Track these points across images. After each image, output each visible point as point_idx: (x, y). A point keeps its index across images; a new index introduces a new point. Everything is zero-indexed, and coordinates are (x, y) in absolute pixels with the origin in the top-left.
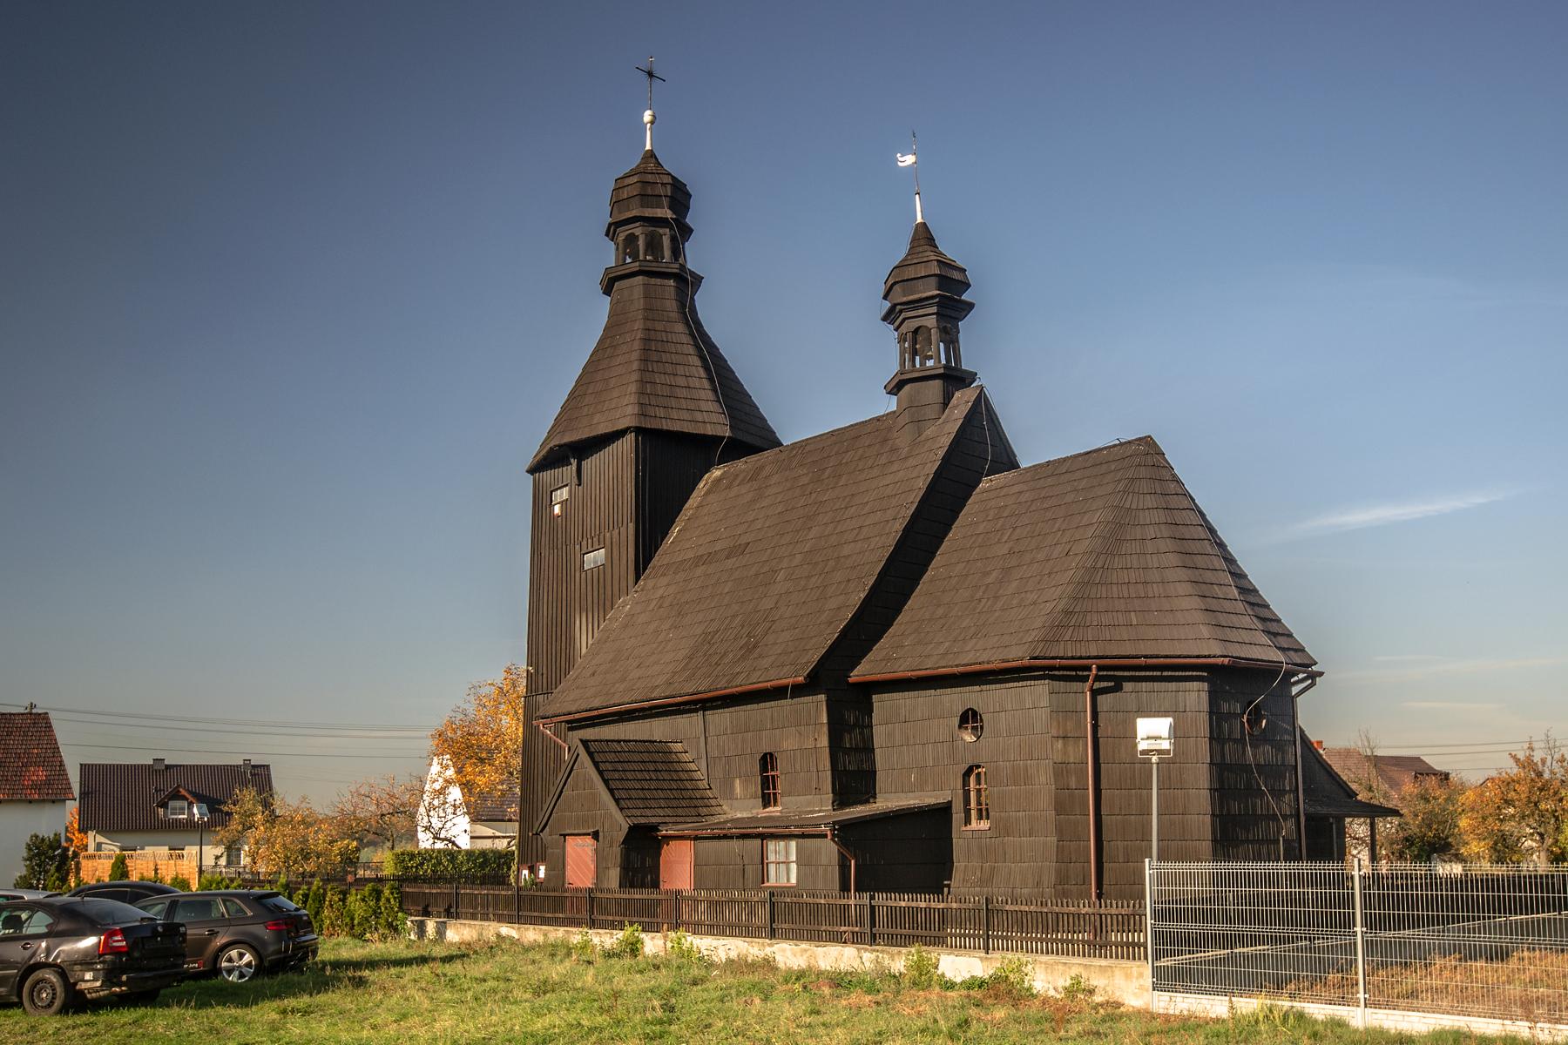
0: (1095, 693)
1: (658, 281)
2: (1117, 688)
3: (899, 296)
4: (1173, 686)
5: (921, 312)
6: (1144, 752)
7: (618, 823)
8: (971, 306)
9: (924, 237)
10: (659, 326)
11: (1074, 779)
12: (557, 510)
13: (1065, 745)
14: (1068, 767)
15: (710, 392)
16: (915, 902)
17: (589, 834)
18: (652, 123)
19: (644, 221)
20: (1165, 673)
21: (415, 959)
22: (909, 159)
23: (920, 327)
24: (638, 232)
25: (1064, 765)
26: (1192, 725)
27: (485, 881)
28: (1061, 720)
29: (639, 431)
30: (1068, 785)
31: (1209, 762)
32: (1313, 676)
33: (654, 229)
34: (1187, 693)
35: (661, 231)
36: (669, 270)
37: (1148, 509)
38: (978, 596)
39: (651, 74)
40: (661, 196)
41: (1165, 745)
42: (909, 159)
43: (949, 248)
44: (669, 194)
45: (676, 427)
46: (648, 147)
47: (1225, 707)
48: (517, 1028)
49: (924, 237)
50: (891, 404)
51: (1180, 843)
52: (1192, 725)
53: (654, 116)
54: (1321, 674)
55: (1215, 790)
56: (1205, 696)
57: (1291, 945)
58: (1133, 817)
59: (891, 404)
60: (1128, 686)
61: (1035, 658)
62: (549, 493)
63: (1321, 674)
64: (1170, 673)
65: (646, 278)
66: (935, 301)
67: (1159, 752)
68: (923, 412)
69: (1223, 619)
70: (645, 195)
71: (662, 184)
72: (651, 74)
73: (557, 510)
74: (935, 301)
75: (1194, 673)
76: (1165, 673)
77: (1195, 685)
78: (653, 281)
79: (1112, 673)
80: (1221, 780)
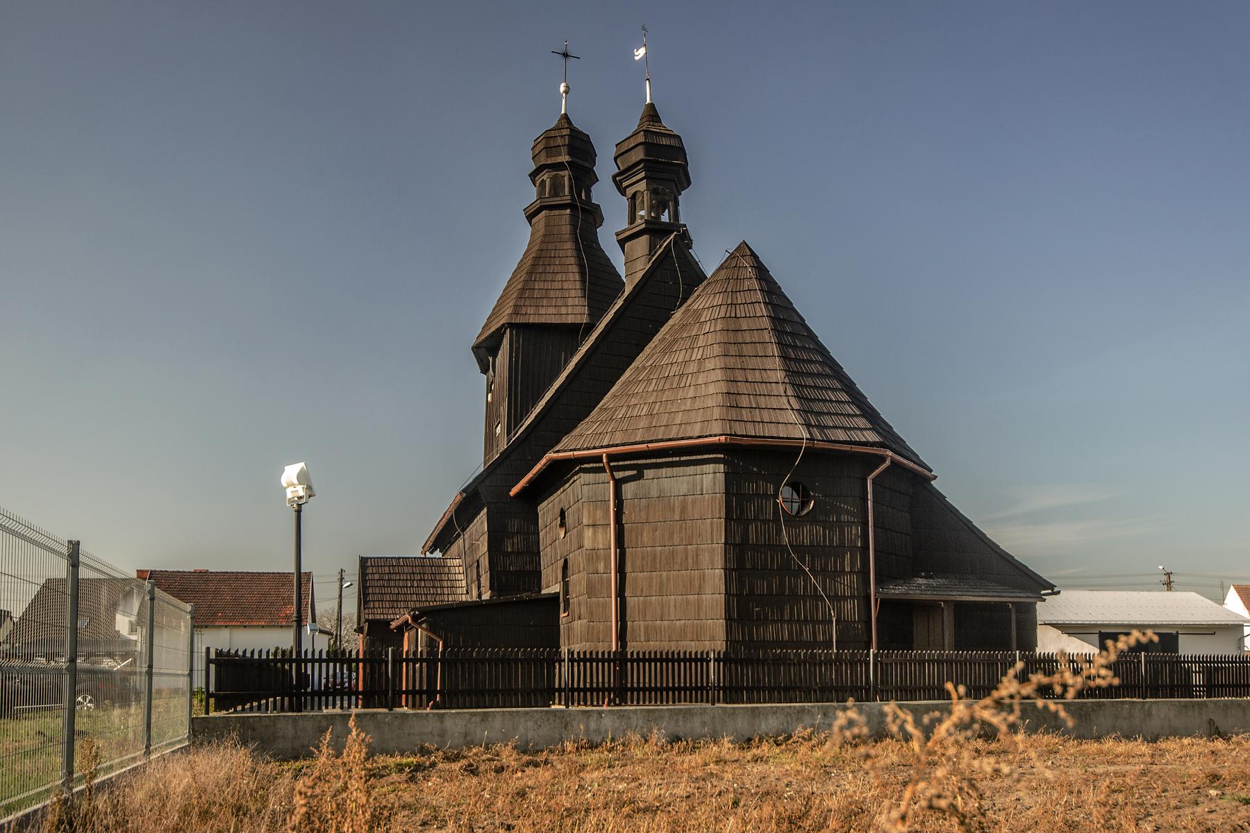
0: (618, 484)
1: (557, 212)
2: (639, 476)
3: (543, 160)
4: (690, 470)
5: (634, 179)
9: (652, 114)
10: (551, 246)
11: (602, 564)
13: (594, 533)
14: (598, 554)
15: (579, 291)
18: (566, 92)
19: (548, 168)
20: (683, 458)
22: (640, 53)
23: (636, 192)
24: (545, 177)
25: (594, 552)
26: (708, 507)
28: (591, 509)
30: (597, 570)
31: (723, 541)
33: (556, 173)
34: (704, 475)
35: (561, 173)
36: (563, 202)
39: (566, 55)
40: (560, 146)
42: (640, 53)
43: (670, 123)
44: (567, 143)
45: (543, 320)
46: (563, 112)
47: (750, 488)
48: (1228, 777)
49: (652, 114)
51: (695, 621)
52: (708, 507)
53: (567, 87)
55: (731, 570)
56: (721, 477)
57: (27, 707)
58: (653, 598)
60: (649, 473)
64: (688, 458)
65: (548, 211)
66: (640, 167)
68: (634, 266)
69: (817, 407)
70: (549, 148)
71: (562, 136)
72: (566, 55)
74: (640, 167)
75: (711, 456)
76: (683, 458)
77: (709, 468)
78: (553, 212)
79: (635, 462)
80: (740, 560)
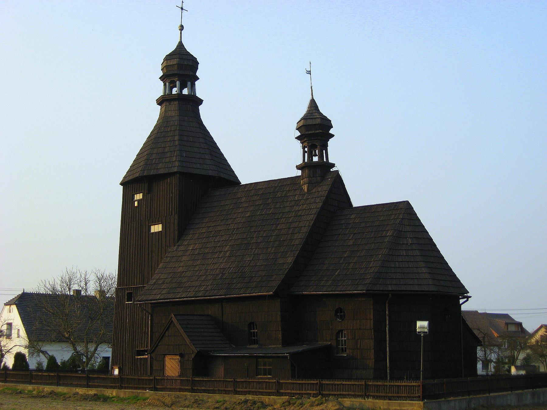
6: (419, 332)
7: (193, 350)
8: (332, 136)
12: (136, 204)
16: (285, 381)
17: (177, 355)
21: (332, 394)
27: (71, 371)
29: (183, 175)
32: (468, 297)
37: (409, 231)
38: (341, 262)
41: (426, 330)
43: (324, 110)
50: (299, 173)
54: (470, 297)
59: (299, 173)
61: (368, 290)
62: (131, 195)
63: (470, 297)
67: (424, 332)
73: (136, 204)
